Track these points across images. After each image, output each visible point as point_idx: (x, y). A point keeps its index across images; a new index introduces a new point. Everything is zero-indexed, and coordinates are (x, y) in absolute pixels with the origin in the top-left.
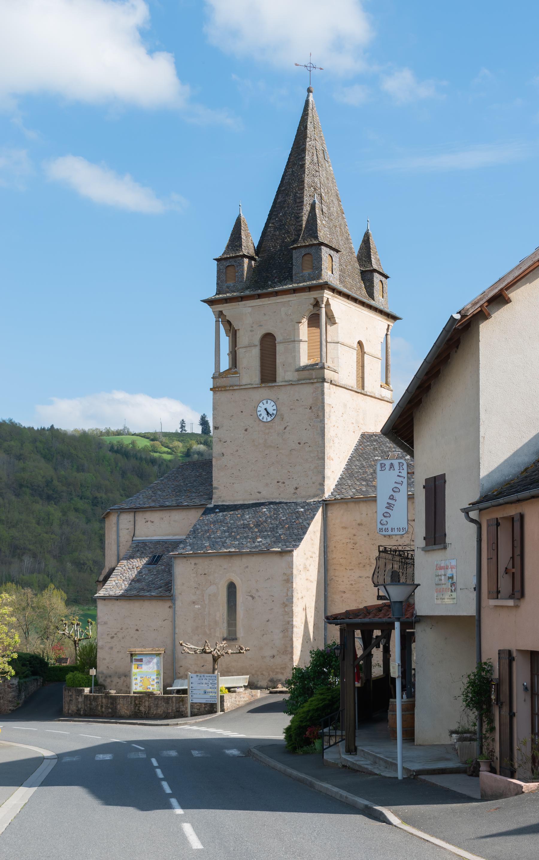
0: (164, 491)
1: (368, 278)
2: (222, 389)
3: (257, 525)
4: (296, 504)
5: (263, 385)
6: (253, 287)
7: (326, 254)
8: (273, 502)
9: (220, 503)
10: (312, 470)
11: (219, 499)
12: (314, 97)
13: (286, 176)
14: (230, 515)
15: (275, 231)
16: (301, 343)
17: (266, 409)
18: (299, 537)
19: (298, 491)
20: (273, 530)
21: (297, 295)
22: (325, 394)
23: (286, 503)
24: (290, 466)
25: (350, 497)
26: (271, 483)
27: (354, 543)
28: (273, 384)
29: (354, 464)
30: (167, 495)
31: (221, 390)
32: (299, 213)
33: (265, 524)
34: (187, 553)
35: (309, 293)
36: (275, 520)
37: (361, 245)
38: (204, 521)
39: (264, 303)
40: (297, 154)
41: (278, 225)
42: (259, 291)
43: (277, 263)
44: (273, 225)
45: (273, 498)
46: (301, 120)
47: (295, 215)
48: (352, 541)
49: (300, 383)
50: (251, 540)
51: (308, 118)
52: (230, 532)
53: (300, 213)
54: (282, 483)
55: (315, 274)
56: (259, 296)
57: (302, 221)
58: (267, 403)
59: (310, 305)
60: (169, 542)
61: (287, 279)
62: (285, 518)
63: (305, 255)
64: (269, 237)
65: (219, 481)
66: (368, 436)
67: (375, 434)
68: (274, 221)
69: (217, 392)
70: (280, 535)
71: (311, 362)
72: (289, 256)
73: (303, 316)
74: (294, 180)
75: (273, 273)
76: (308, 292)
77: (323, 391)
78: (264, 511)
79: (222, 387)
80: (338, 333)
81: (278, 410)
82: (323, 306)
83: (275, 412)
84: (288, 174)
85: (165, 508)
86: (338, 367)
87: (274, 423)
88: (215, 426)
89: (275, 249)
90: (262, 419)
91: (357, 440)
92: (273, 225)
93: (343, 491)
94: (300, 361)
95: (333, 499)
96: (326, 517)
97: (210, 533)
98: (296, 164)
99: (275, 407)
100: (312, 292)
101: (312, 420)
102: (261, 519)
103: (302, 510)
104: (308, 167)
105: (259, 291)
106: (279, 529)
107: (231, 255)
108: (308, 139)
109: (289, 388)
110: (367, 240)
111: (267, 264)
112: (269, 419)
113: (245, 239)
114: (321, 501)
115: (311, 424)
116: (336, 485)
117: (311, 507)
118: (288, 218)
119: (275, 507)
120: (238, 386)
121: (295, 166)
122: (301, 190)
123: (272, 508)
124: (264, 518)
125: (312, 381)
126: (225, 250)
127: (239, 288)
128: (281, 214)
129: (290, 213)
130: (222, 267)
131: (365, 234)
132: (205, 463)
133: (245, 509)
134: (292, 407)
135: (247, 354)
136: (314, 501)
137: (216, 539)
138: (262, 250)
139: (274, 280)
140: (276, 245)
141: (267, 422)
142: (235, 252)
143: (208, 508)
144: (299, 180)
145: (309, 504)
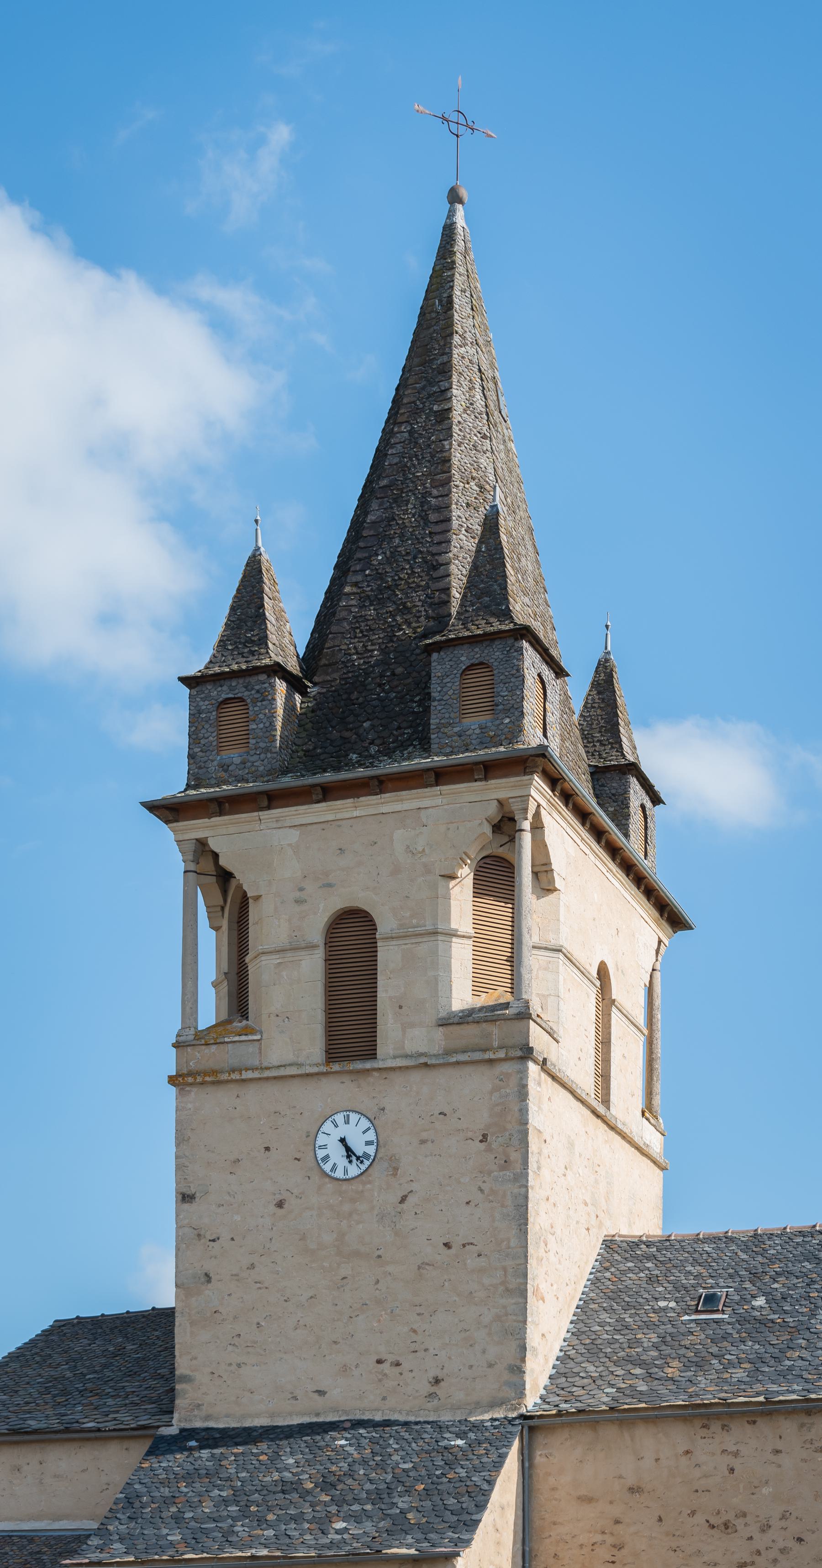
0: (16, 1392)
1: (613, 791)
2: (207, 1079)
3: (326, 1484)
4: (438, 1426)
5: (336, 1067)
6: (301, 769)
7: (533, 669)
8: (363, 1420)
9: (198, 1424)
10: (486, 1326)
11: (196, 1412)
12: (467, 218)
13: (392, 448)
14: (235, 1455)
15: (362, 607)
16: (454, 939)
17: (343, 1140)
18: (465, 1517)
19: (441, 1390)
20: (377, 1497)
21: (445, 788)
22: (530, 1097)
23: (406, 1424)
24: (419, 1314)
25: (604, 1407)
26: (357, 1366)
27: (614, 1546)
28: (368, 1065)
29: (597, 1320)
30: (27, 1403)
31: (203, 1083)
32: (436, 554)
33: (350, 1481)
34: (118, 1560)
35: (483, 783)
36: (379, 1471)
37: (589, 695)
38: (156, 1472)
39: (339, 816)
40: (424, 383)
41: (372, 590)
42: (329, 777)
43: (375, 699)
44: (355, 590)
45: (363, 1411)
46: (430, 284)
47: (425, 561)
48: (610, 1540)
49: (454, 1060)
50: (314, 1526)
51: (453, 275)
52: (242, 1503)
53: (440, 554)
54: (392, 1364)
55: (502, 727)
56: (327, 793)
57: (449, 575)
58: (347, 1122)
59: (484, 821)
60: (40, 1537)
61: (409, 746)
62: (411, 1465)
63: (468, 668)
64: (345, 624)
65: (196, 1358)
66: (625, 1244)
67: (644, 1239)
68: (359, 578)
69: (188, 1089)
70: (403, 1512)
71: (484, 1000)
72: (410, 680)
73: (464, 856)
74: (416, 456)
75: (361, 731)
76: (480, 780)
77: (525, 1086)
78: (342, 1446)
79: (206, 1073)
80: (558, 920)
81: (381, 1142)
82: (526, 825)
83: (371, 1150)
84: (397, 441)
85: (26, 1437)
86: (558, 1023)
87: (370, 1182)
88: (184, 1190)
89: (366, 660)
90: (331, 1171)
91: (595, 1257)
92: (355, 590)
93: (578, 1392)
94: (450, 997)
95: (554, 1412)
96: (531, 1466)
97: (179, 1506)
98: (422, 410)
99: (371, 1136)
100: (493, 781)
101: (490, 1173)
102: (334, 1468)
103: (460, 1442)
104: (460, 419)
105: (329, 777)
106: (396, 1494)
107: (235, 667)
108: (456, 339)
109: (415, 1077)
110: (606, 681)
111: (342, 703)
112: (354, 1170)
113: (274, 622)
114: (514, 1419)
115: (483, 1186)
116: (551, 1377)
117: (487, 1434)
118: (403, 569)
119: (374, 1434)
120: (257, 1069)
121: (420, 417)
122: (442, 485)
123: (365, 1438)
124: (344, 1465)
125: (490, 1055)
126: (214, 655)
127: (261, 768)
128: (380, 558)
129: (408, 554)
130: (204, 705)
131: (599, 664)
132: (128, 1320)
133: (281, 1439)
134: (424, 1135)
135: (284, 973)
136: (493, 1420)
137: (201, 1523)
138: (324, 661)
139: (367, 749)
140: (369, 648)
141: (346, 1180)
142: (245, 659)
143: (162, 1438)
144: (433, 456)
145: (477, 1427)
